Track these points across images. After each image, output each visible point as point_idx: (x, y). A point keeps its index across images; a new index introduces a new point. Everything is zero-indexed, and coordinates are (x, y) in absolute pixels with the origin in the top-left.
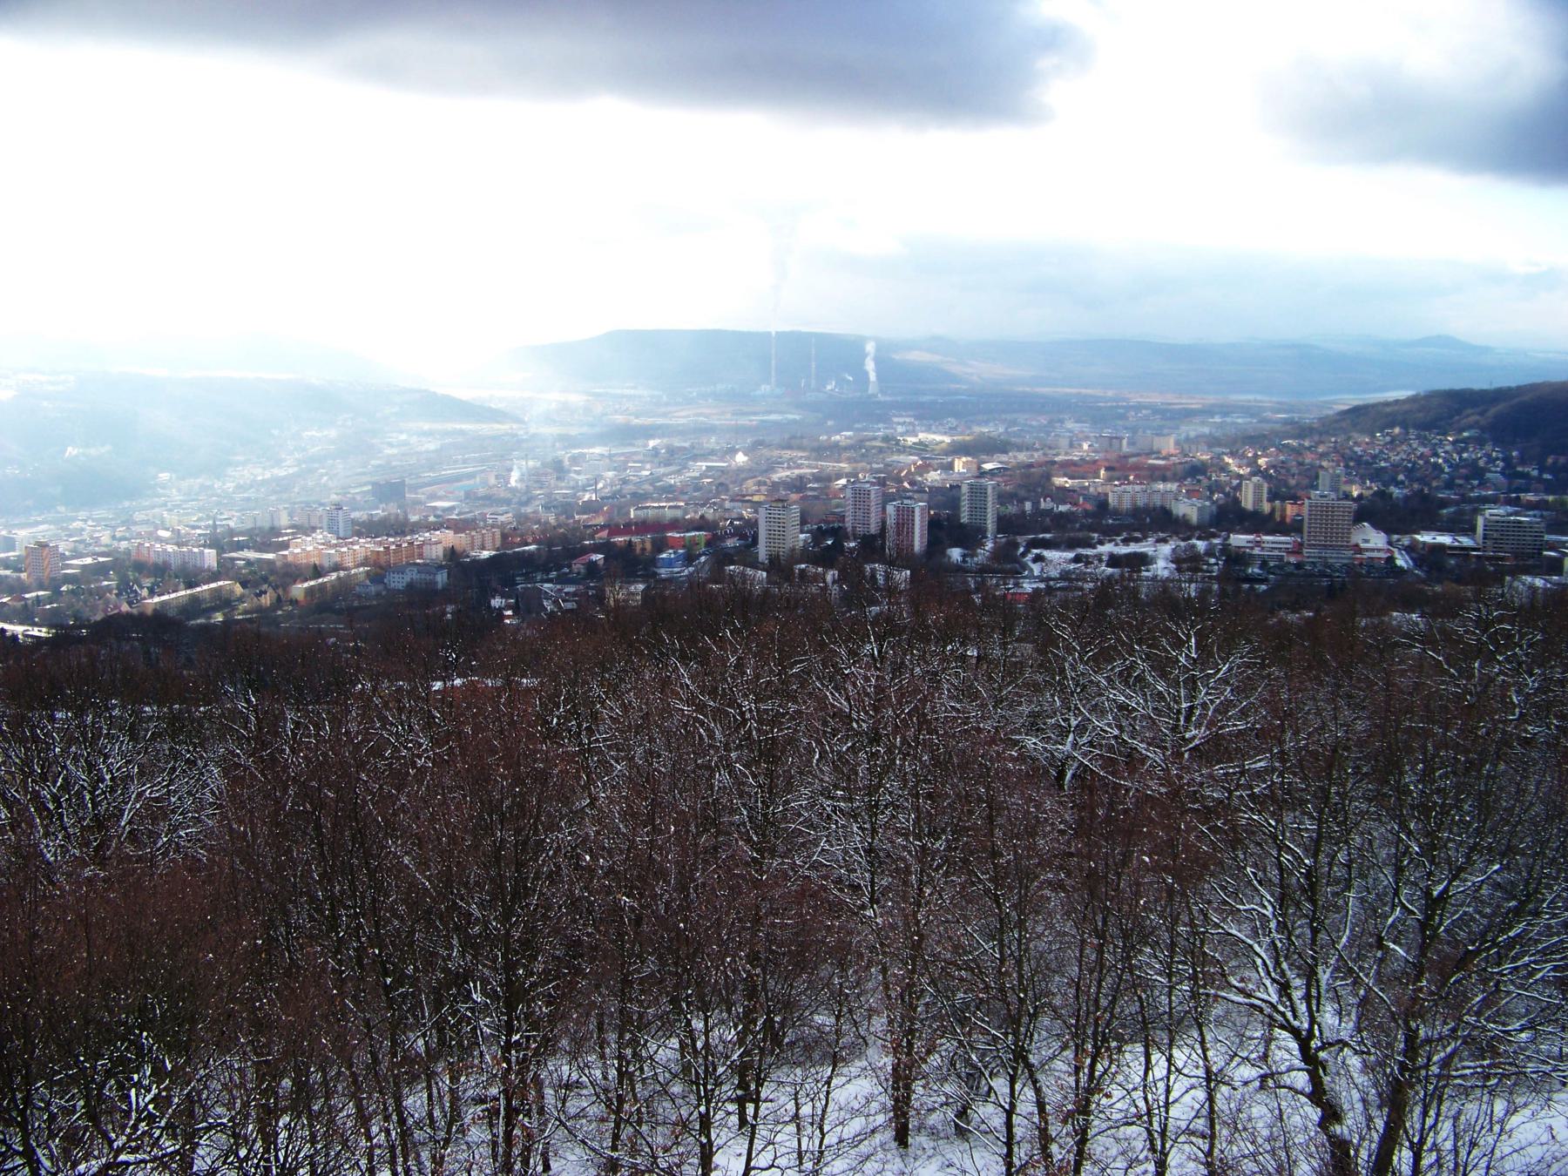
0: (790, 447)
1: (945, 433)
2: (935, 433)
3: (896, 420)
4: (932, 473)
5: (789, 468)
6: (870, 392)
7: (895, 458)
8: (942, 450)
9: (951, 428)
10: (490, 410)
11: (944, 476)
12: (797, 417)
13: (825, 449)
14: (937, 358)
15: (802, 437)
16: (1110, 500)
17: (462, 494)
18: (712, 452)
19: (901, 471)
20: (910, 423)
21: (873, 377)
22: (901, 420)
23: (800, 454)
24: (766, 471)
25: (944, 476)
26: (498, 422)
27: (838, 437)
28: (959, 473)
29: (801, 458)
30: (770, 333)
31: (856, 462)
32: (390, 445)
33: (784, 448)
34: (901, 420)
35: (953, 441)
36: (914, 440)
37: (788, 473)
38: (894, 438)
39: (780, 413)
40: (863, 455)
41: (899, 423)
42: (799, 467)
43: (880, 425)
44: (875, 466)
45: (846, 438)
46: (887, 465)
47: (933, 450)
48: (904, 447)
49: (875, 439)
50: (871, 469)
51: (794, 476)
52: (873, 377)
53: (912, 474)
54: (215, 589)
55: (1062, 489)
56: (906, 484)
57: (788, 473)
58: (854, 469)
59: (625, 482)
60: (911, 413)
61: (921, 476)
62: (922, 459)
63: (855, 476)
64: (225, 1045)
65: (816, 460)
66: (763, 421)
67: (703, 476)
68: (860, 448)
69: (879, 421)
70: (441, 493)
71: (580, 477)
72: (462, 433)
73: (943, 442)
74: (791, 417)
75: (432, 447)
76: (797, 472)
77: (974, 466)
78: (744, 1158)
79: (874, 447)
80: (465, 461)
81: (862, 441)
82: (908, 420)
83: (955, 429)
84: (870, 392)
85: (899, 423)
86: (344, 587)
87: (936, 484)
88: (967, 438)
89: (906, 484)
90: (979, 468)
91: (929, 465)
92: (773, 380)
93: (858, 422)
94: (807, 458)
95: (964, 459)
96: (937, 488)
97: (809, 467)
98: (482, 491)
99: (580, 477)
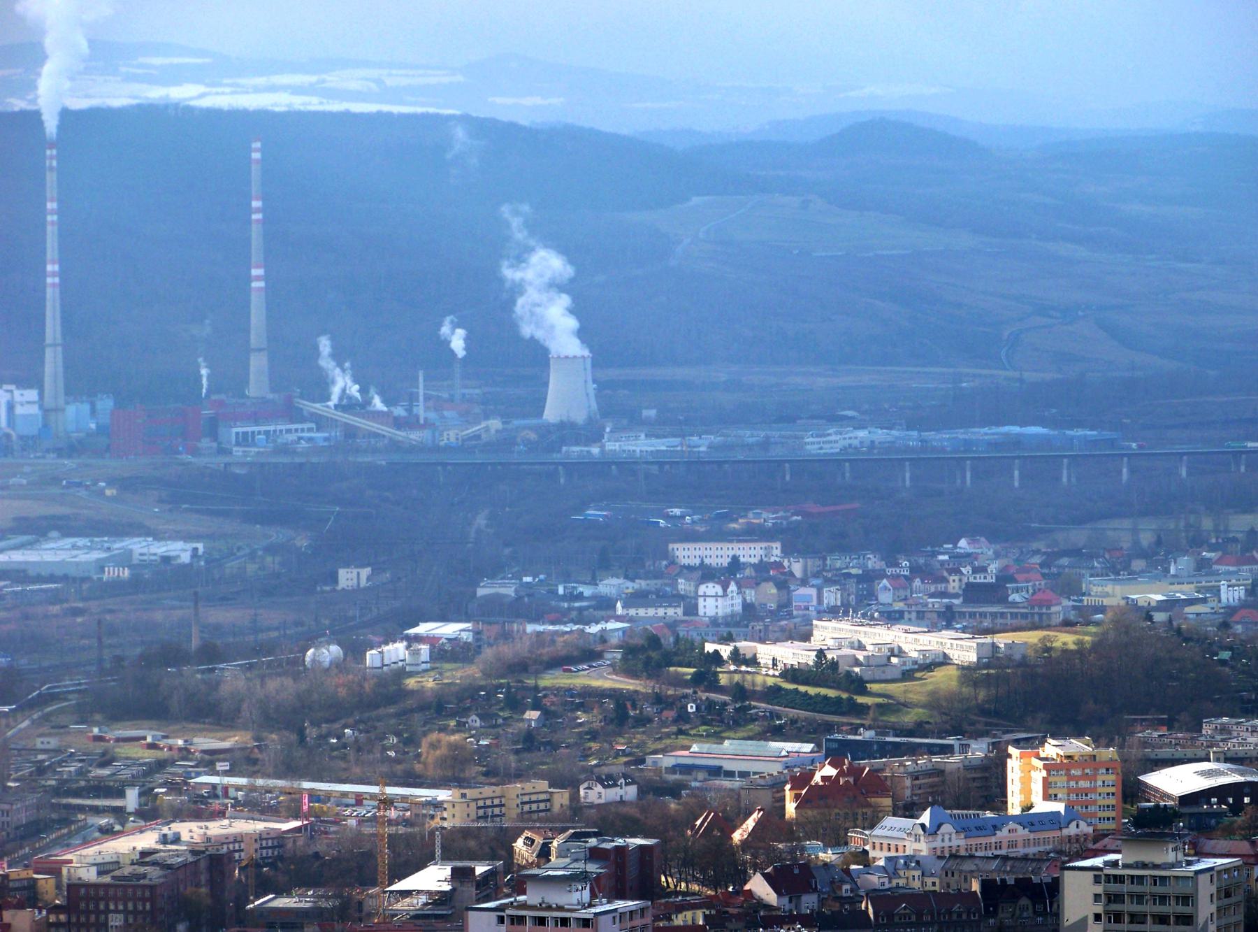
1: (947, 619)
2: (892, 618)
3: (687, 553)
4: (892, 826)
5: (149, 814)
6: (551, 414)
7: (698, 750)
8: (935, 702)
9: (974, 593)
11: (951, 838)
12: (181, 551)
13: (335, 711)
15: (211, 654)
16: (520, 301)
19: (729, 822)
20: (762, 568)
22: (718, 554)
23: (204, 742)
24: (34, 830)
25: (951, 838)
27: (396, 651)
28: (1030, 820)
29: (209, 761)
31: (494, 774)
33: (121, 711)
34: (718, 554)
35: (992, 658)
36: (793, 654)
37: (147, 840)
38: (687, 651)
40: (529, 741)
41: (707, 573)
43: (610, 585)
44: (594, 794)
45: (445, 653)
46: (654, 789)
47: (892, 706)
48: (740, 692)
49: (589, 654)
50: (577, 809)
51: (177, 854)
53: (788, 831)
54: (418, 397)
56: (759, 886)
57: (147, 840)
58: (486, 811)
60: (767, 518)
61: (836, 839)
62: (835, 755)
63: (500, 846)
64: (503, 423)
65: (289, 769)
68: (516, 704)
69: (603, 565)
73: (945, 661)
74: (144, 548)
76: (190, 831)
77: (1106, 785)
78: (534, 791)
79: (588, 698)
81: (521, 667)
82: (750, 553)
83: (992, 593)
84: (551, 414)
85: (707, 573)
87: (914, 881)
88: (1066, 640)
89: (759, 886)
90: (1132, 791)
91: (877, 784)
92: (52, 362)
93: (495, 570)
94: (243, 762)
95: (1051, 749)
96: (919, 900)
97: (254, 806)
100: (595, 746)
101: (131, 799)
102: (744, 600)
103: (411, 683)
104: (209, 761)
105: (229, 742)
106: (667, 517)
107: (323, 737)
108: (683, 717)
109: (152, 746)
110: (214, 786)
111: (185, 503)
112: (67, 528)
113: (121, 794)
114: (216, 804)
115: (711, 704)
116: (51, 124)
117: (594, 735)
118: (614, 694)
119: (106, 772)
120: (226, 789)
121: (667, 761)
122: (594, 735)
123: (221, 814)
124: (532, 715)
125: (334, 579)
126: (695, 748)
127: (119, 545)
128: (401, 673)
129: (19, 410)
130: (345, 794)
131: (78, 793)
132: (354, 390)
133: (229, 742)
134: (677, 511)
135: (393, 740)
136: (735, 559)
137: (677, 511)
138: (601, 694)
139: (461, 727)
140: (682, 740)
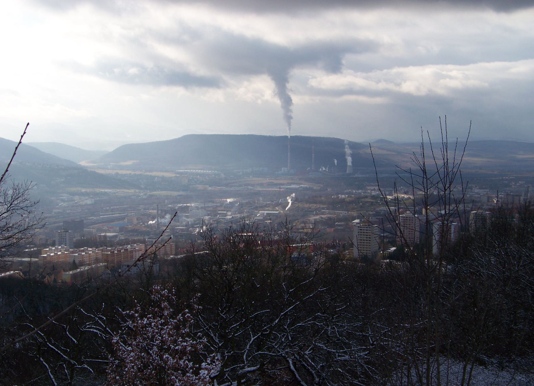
0: (315, 203)
3: (368, 188)
5: (317, 214)
6: (347, 172)
10: (101, 176)
14: (385, 152)
17: (118, 229)
18: (266, 206)
21: (349, 163)
23: (322, 206)
26: (126, 189)
29: (323, 208)
30: (287, 137)
32: (63, 201)
33: (310, 203)
39: (297, 184)
40: (361, 207)
42: (323, 213)
46: (377, 212)
52: (349, 163)
55: (266, 363)
59: (218, 222)
65: (333, 209)
66: (287, 188)
67: (265, 218)
70: (105, 228)
71: (188, 220)
72: (105, 194)
75: (89, 202)
79: (367, 202)
80: (112, 210)
86: (89, 277)
97: (329, 213)
98: (130, 227)
99: (188, 220)
100: (369, 207)
101: (315, 212)
102: (216, 224)
103: (346, 200)
104: (323, 208)
105: (325, 206)
106: (366, 184)
107: (336, 206)
108: (379, 204)
109: (315, 207)
110: (324, 211)
111: (229, 198)
112: (294, 184)
113: (313, 212)
114: (325, 213)
115: (383, 203)
116: (289, 137)
117: (369, 206)
118: (371, 202)
119: (310, 210)
120: (326, 212)
121: (379, 209)
122: (369, 206)
123: (326, 214)
124: (361, 204)
125: (327, 190)
126: (382, 208)
127: (301, 186)
128: (344, 199)
129: (285, 170)
130: (340, 212)
131: (307, 212)
132: (325, 169)
133: (325, 206)
134: (366, 183)
135: (345, 206)
136: (374, 188)
137: (366, 183)
138: (369, 202)
139: (353, 205)
140: (380, 207)
